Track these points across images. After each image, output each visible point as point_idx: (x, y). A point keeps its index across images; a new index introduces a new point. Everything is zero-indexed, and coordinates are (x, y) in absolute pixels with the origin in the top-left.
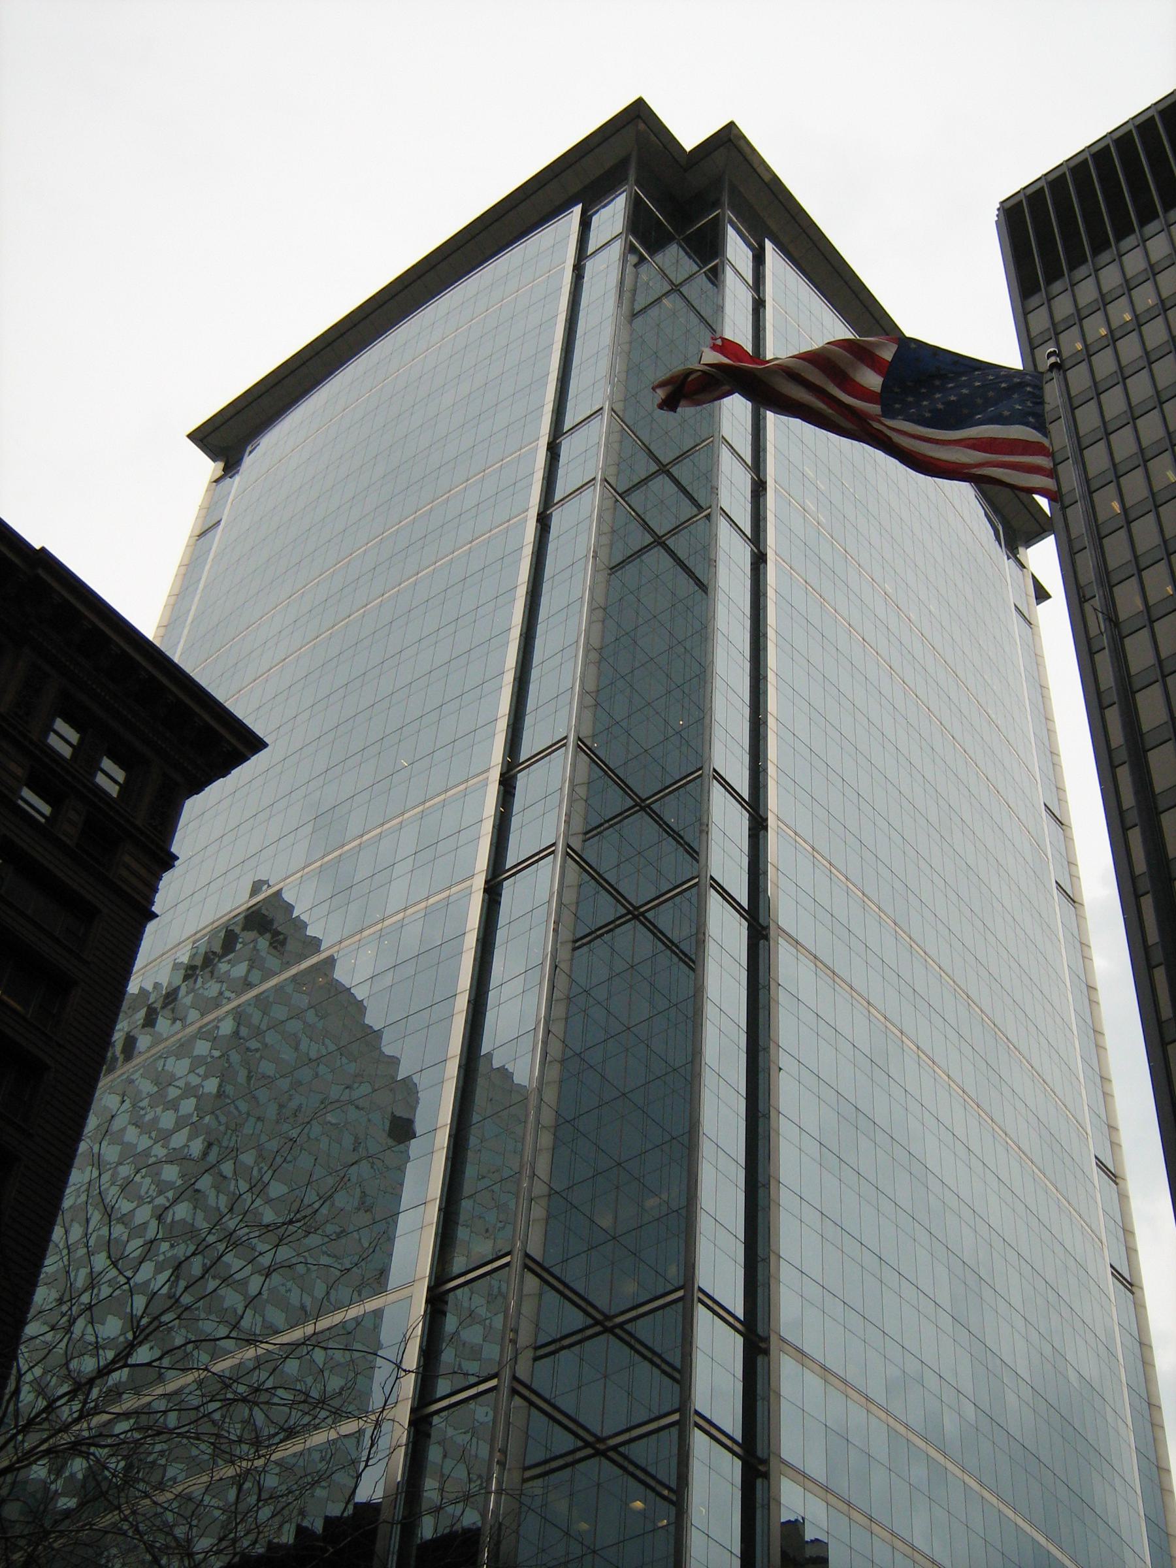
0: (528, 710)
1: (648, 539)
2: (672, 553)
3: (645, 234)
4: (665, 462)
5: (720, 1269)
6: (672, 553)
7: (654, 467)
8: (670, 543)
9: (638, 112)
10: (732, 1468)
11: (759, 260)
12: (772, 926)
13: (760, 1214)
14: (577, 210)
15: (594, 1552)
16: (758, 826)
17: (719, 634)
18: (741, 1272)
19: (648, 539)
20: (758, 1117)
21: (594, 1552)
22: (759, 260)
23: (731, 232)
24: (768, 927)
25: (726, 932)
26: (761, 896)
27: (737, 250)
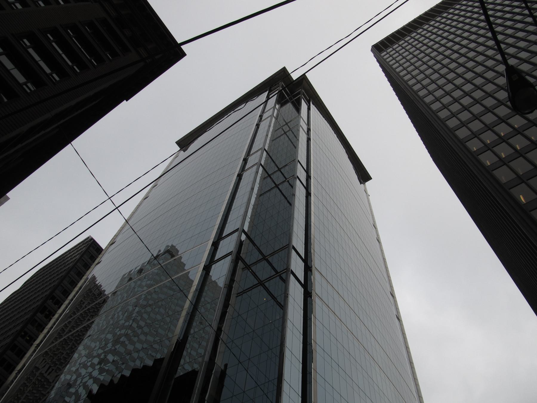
0: (236, 197)
1: (256, 282)
2: (270, 264)
3: (281, 101)
4: (262, 279)
5: (298, 242)
6: (270, 264)
7: (261, 257)
8: (267, 284)
9: (284, 68)
10: (304, 191)
11: (309, 109)
12: (313, 267)
13: (308, 355)
14: (266, 93)
15: (249, 359)
16: (308, 195)
17: (285, 382)
18: (301, 366)
19: (261, 257)
20: (307, 345)
21: (244, 392)
22: (309, 109)
23: (303, 101)
24: (312, 267)
25: (296, 292)
26: (309, 282)
27: (304, 106)
